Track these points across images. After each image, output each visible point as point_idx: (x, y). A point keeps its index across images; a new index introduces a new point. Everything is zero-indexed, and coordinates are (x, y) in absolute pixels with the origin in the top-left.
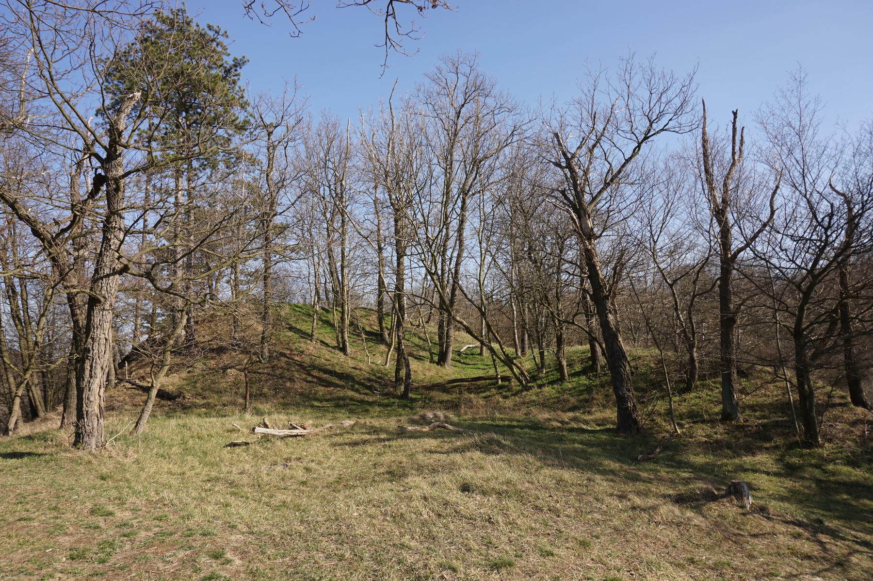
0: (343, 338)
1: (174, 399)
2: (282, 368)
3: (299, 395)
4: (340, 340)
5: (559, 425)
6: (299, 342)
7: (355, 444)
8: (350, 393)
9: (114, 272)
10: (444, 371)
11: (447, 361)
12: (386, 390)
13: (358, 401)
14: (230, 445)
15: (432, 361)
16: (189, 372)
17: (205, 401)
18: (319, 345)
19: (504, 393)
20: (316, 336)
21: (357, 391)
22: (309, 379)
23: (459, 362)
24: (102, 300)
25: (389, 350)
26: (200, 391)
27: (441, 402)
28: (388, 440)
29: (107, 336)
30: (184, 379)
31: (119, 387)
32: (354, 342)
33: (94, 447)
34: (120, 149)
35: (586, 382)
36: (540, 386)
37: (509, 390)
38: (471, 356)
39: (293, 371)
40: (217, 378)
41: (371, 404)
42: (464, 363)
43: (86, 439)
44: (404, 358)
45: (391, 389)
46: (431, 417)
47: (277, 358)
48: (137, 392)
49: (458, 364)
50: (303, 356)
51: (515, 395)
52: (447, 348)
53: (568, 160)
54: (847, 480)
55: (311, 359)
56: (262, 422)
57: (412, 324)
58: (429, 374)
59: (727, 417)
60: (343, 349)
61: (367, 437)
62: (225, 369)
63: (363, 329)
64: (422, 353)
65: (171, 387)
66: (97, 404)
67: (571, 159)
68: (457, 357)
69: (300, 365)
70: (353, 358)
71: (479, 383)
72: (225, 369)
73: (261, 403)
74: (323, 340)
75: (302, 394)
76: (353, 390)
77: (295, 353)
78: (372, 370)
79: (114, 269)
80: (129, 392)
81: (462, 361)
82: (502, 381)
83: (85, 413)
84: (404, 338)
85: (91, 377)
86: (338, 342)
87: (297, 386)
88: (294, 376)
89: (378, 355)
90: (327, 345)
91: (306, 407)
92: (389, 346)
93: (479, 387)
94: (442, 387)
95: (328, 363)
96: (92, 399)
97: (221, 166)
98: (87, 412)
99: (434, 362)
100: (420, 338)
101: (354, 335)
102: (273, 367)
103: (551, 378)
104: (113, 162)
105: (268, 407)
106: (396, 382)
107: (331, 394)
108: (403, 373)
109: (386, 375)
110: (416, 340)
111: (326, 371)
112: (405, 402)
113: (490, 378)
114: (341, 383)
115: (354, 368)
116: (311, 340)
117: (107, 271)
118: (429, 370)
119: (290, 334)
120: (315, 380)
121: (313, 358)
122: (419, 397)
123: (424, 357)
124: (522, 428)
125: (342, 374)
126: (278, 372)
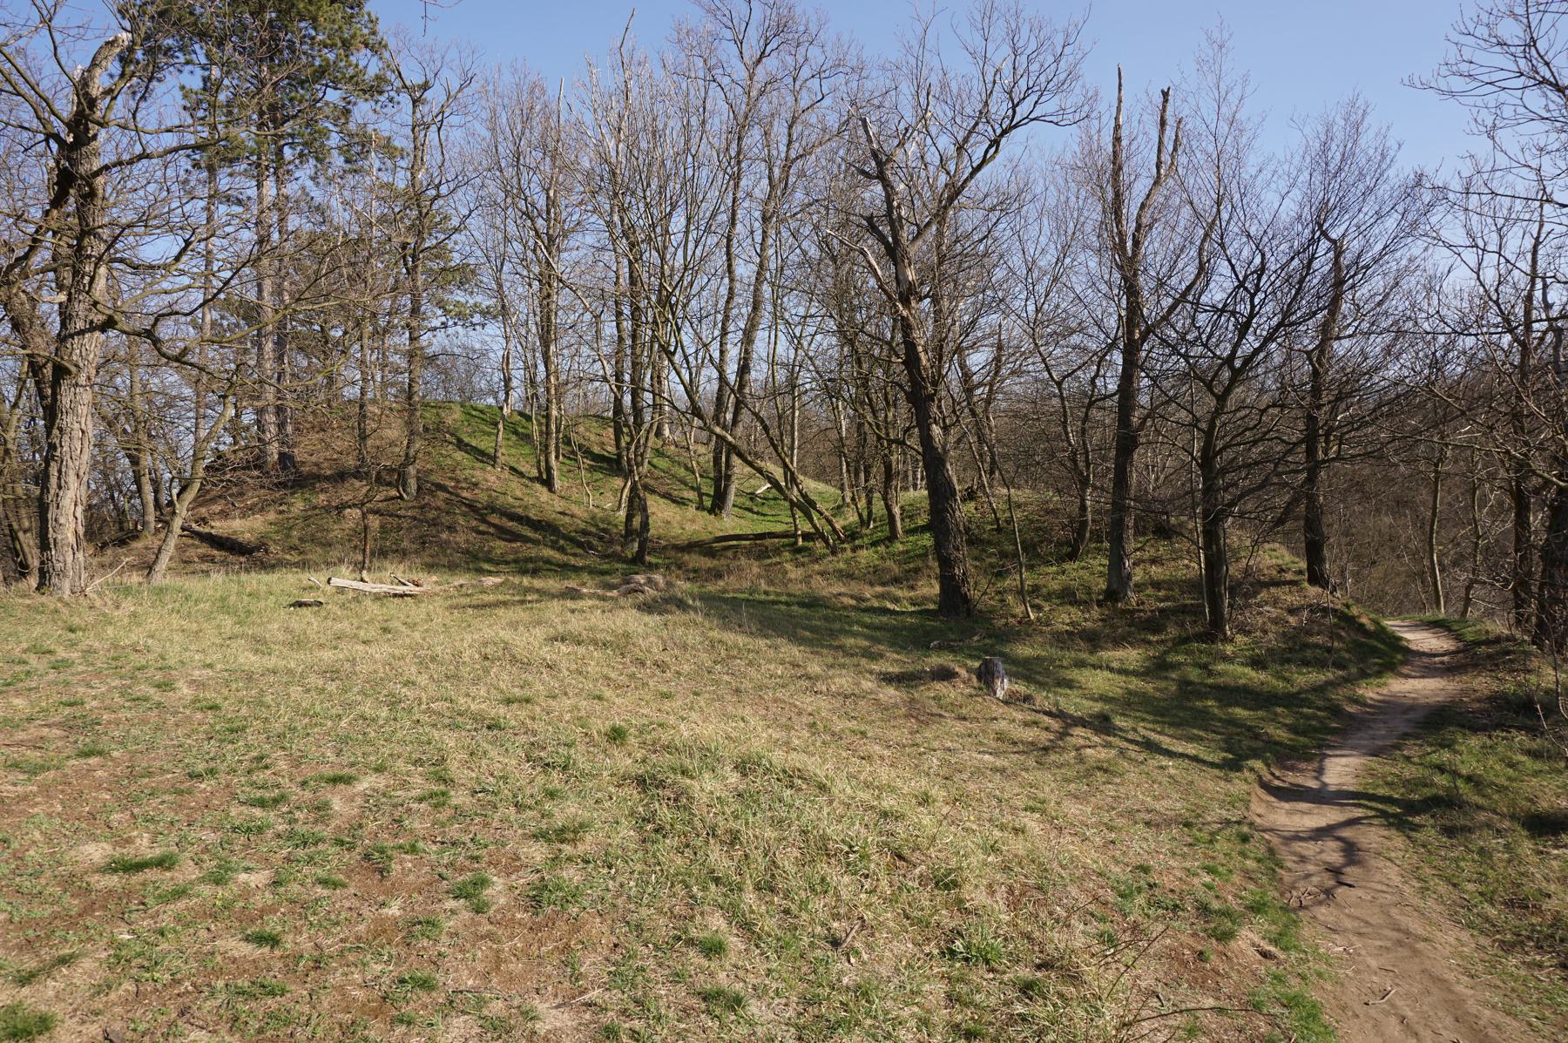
0: (547, 461)
2: (437, 509)
5: (853, 602)
6: (473, 468)
8: (548, 552)
9: (92, 328)
13: (558, 565)
14: (293, 605)
15: (701, 507)
16: (281, 512)
18: (506, 474)
20: (501, 459)
21: (562, 550)
22: (483, 527)
23: (750, 510)
24: (73, 369)
26: (297, 542)
29: (83, 427)
33: (68, 592)
34: (93, 129)
38: (772, 502)
42: (758, 513)
43: (55, 580)
47: (431, 492)
48: (191, 541)
52: (727, 486)
53: (880, 164)
54: (1233, 684)
55: (490, 496)
58: (689, 527)
59: (1112, 595)
60: (548, 483)
62: (341, 508)
65: (247, 536)
66: (72, 529)
67: (885, 163)
68: (748, 504)
71: (768, 542)
72: (341, 508)
74: (516, 466)
76: (553, 548)
77: (464, 485)
78: (593, 518)
79: (92, 322)
81: (755, 509)
82: (804, 540)
83: (51, 541)
85: (60, 487)
87: (460, 538)
89: (608, 494)
90: (521, 475)
95: (517, 503)
96: (62, 520)
97: (338, 161)
102: (422, 507)
104: (84, 149)
108: (637, 522)
111: (513, 517)
114: (537, 536)
117: (80, 325)
118: (693, 521)
119: (459, 455)
120: (491, 530)
121: (494, 494)
125: (539, 521)
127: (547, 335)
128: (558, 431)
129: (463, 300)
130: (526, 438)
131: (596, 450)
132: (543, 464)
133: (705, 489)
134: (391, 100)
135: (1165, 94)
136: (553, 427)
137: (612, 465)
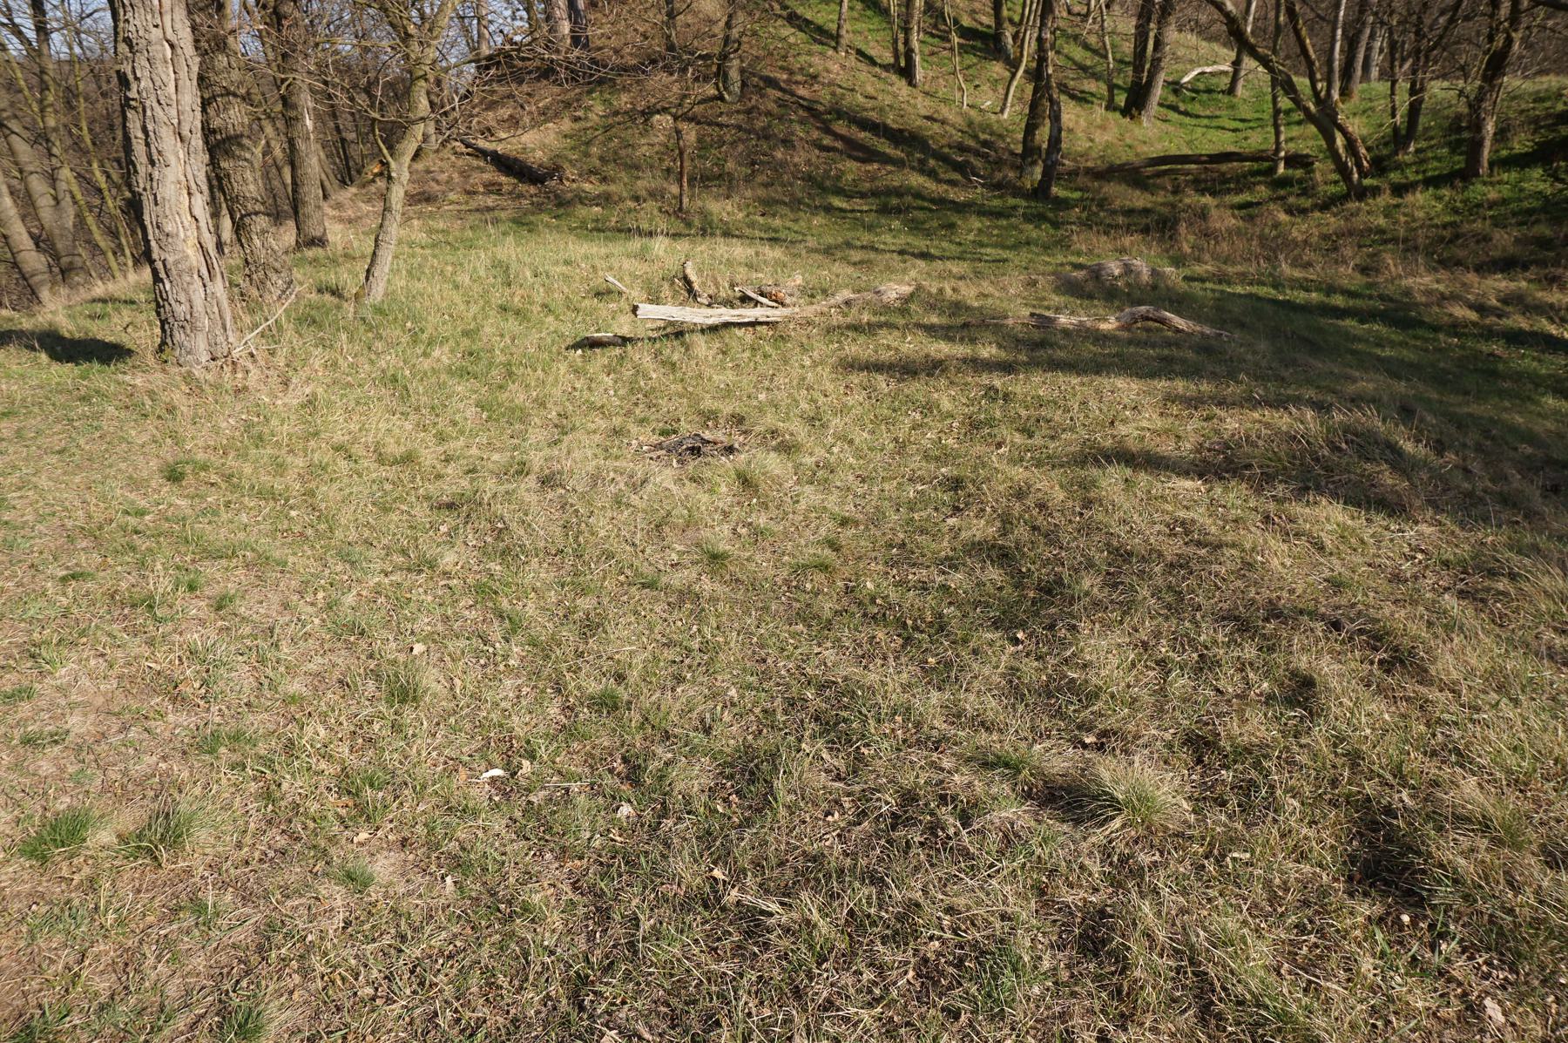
0: (907, 42)
1: (542, 183)
2: (769, 113)
3: (803, 179)
4: (901, 47)
5: (1473, 316)
6: (809, 53)
7: (906, 369)
8: (916, 180)
10: (1137, 132)
11: (1149, 107)
12: (998, 176)
13: (933, 201)
15: (1111, 106)
16: (577, 119)
17: (603, 188)
18: (852, 61)
19: (1292, 200)
20: (846, 38)
21: (932, 174)
22: (827, 141)
23: (1174, 108)
25: (1014, 75)
26: (597, 163)
27: (1129, 212)
28: (1007, 368)
30: (565, 136)
31: (446, 153)
32: (932, 54)
33: (204, 358)
35: (1546, 187)
36: (1399, 190)
37: (1305, 193)
38: (1205, 96)
39: (791, 121)
40: (632, 134)
41: (961, 208)
42: (1186, 113)
44: (1051, 100)
45: (1011, 175)
46: (1117, 272)
47: (760, 91)
49: (1173, 116)
50: (816, 87)
51: (1324, 207)
55: (833, 94)
56: (680, 276)
57: (1069, 12)
58: (1101, 138)
60: (907, 73)
61: (941, 349)
62: (648, 113)
63: (956, 22)
64: (1090, 86)
65: (539, 154)
66: (193, 241)
68: (1172, 98)
69: (809, 109)
70: (927, 94)
71: (1224, 167)
73: (716, 198)
74: (863, 48)
75: (809, 178)
76: (922, 172)
77: (799, 78)
78: (970, 124)
80: (460, 163)
81: (1182, 107)
82: (1287, 166)
84: (1053, 47)
86: (897, 57)
88: (792, 134)
90: (872, 61)
91: (815, 210)
92: (1013, 65)
93: (1224, 179)
94: (1133, 174)
98: (164, 262)
99: (1115, 109)
100: (1086, 47)
101: (933, 36)
102: (749, 112)
103: (1433, 169)
105: (729, 208)
106: (1023, 156)
107: (873, 179)
108: (1043, 134)
109: (1001, 136)
110: (1078, 54)
111: (865, 125)
112: (1040, 206)
113: (1256, 157)
114: (897, 153)
115: (928, 118)
116: (835, 49)
118: (1103, 128)
119: (788, 31)
121: (839, 91)
122: (1077, 195)
123: (1092, 95)
124: (1364, 316)
125: (901, 131)
126: (760, 123)
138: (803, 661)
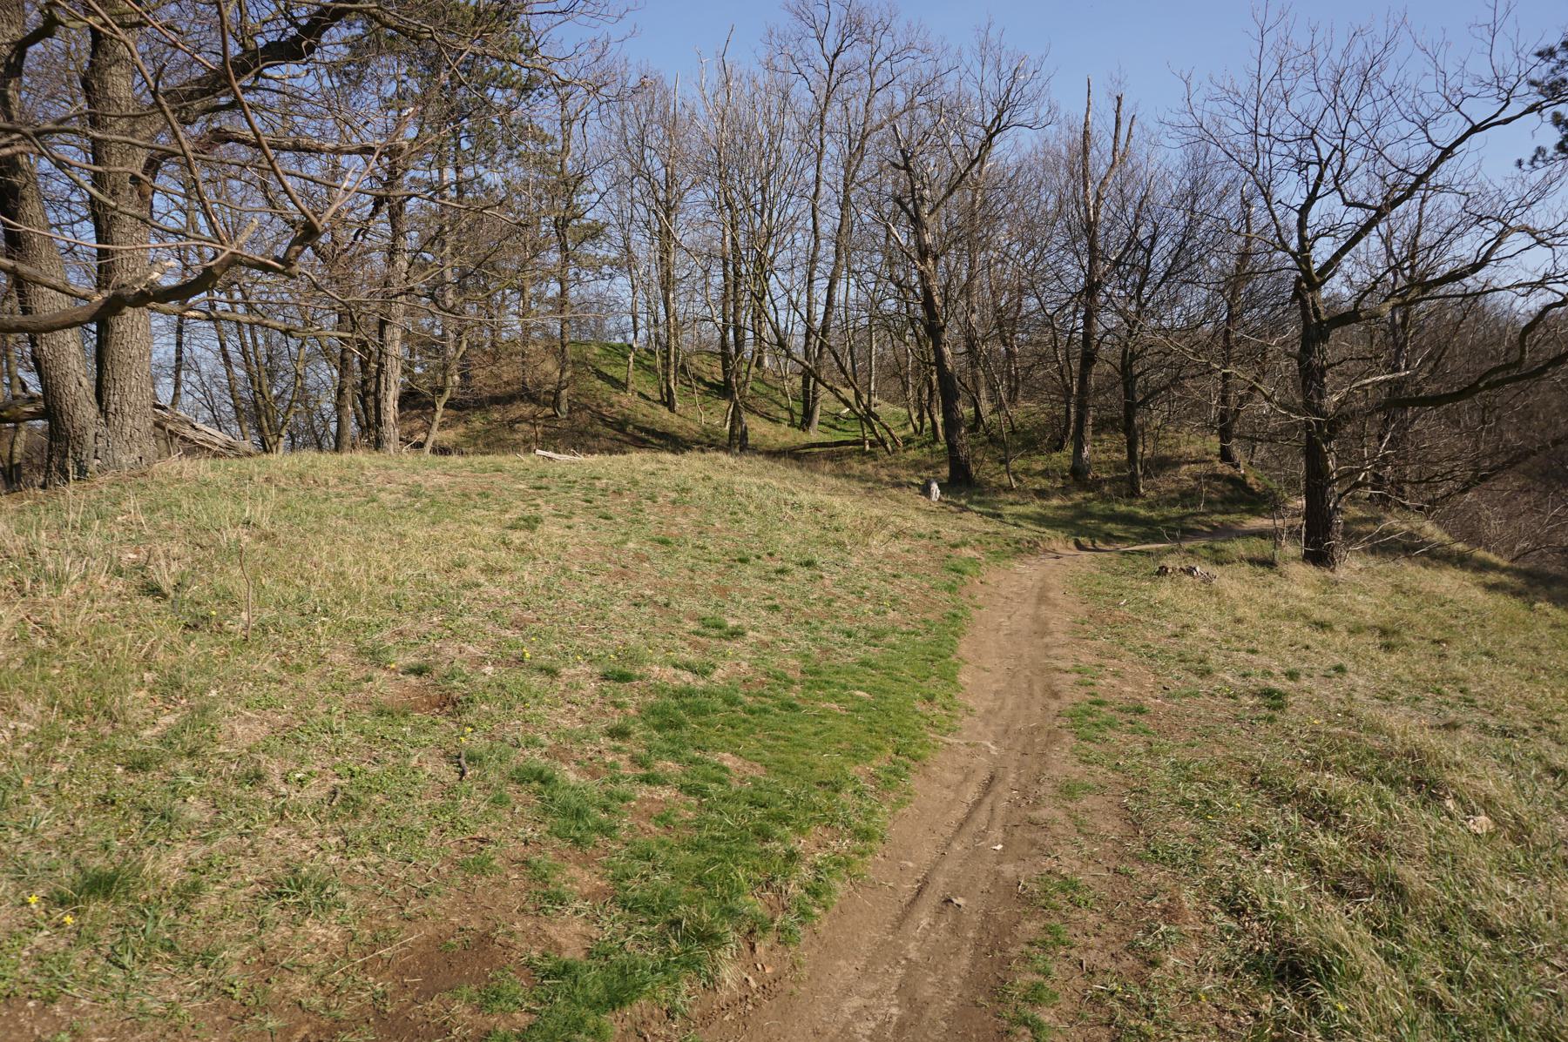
15: (792, 424)
52: (814, 407)
53: (906, 159)
58: (782, 440)
60: (669, 404)
71: (842, 448)
72: (513, 422)
78: (705, 430)
118: (785, 435)
119: (598, 383)
127: (667, 283)
128: (676, 362)
129: (1055, 456)
130: (651, 369)
131: (708, 379)
132: (665, 390)
133: (797, 410)
134: (541, 95)
135: (1119, 99)
136: (672, 359)
137: (723, 390)
138: (489, 296)
